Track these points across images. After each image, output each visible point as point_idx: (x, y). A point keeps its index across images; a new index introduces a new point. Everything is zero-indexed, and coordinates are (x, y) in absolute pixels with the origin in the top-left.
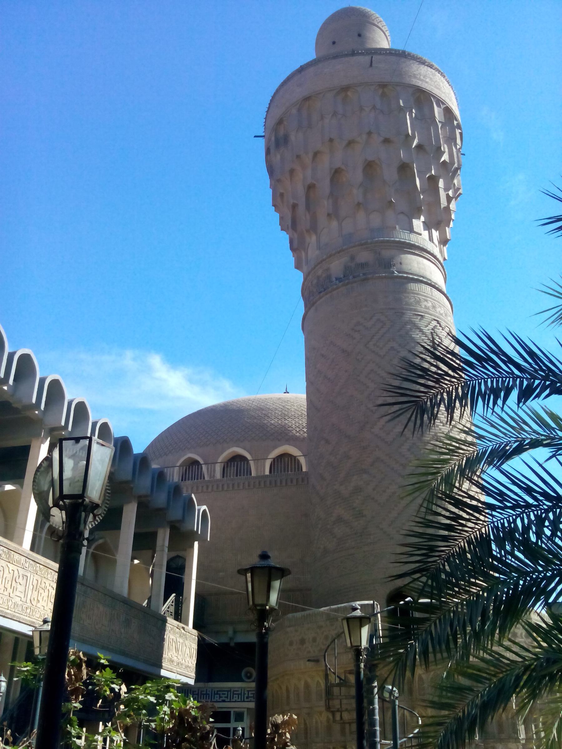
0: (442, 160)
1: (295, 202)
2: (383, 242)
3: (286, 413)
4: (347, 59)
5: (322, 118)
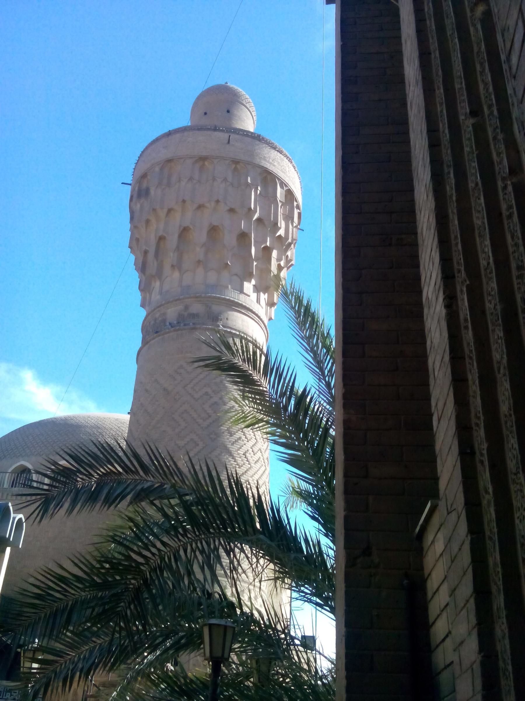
0: (278, 234)
2: (215, 298)
4: (209, 133)
5: (180, 180)
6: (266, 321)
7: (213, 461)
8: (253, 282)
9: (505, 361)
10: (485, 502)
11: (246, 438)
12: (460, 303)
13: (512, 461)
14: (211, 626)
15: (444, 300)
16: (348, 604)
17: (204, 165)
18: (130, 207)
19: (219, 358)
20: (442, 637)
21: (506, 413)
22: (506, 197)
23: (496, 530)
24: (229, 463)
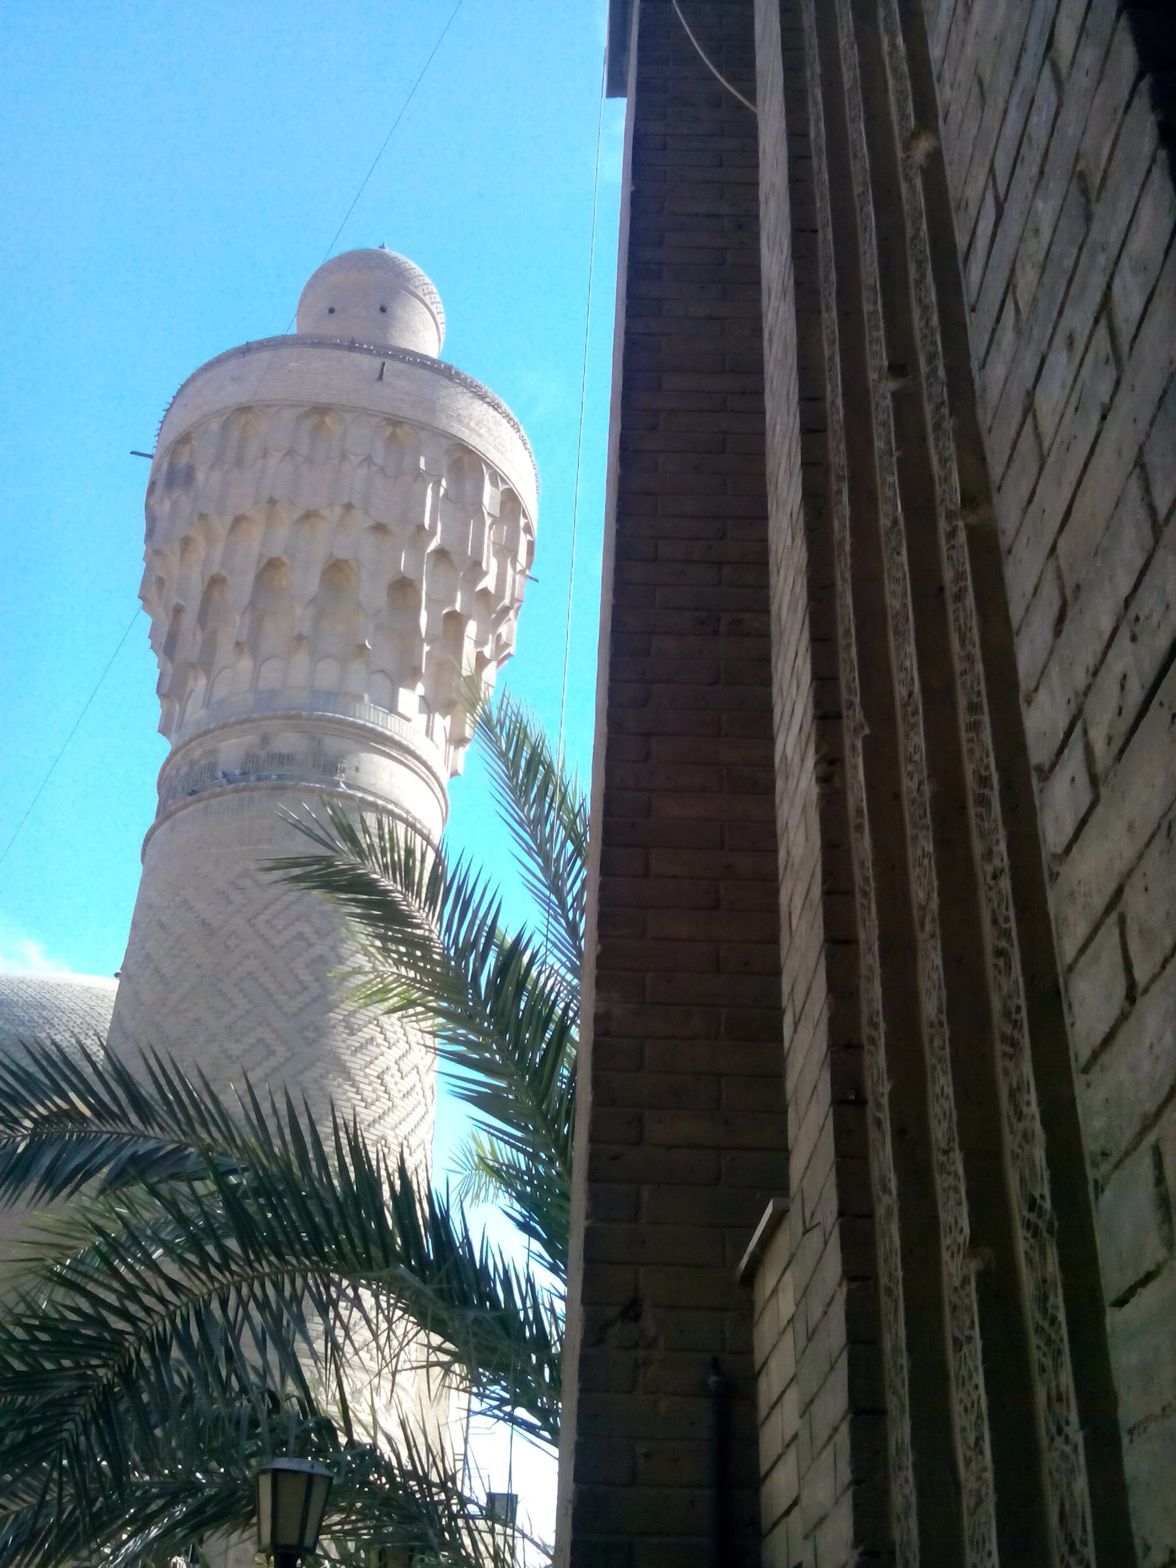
1: (182, 602)
2: (331, 720)
3: (93, 1022)
4: (337, 353)
5: (265, 455)
6: (444, 775)
7: (304, 1091)
8: (420, 689)
9: (935, 904)
10: (880, 1211)
11: (385, 1039)
12: (849, 775)
13: (939, 1122)
14: (276, 1473)
15: (816, 764)
16: (582, 1431)
17: (322, 423)
18: (148, 507)
19: (327, 862)
20: (785, 1507)
21: (933, 1017)
22: (954, 553)
23: (900, 1274)
24: (344, 1097)
